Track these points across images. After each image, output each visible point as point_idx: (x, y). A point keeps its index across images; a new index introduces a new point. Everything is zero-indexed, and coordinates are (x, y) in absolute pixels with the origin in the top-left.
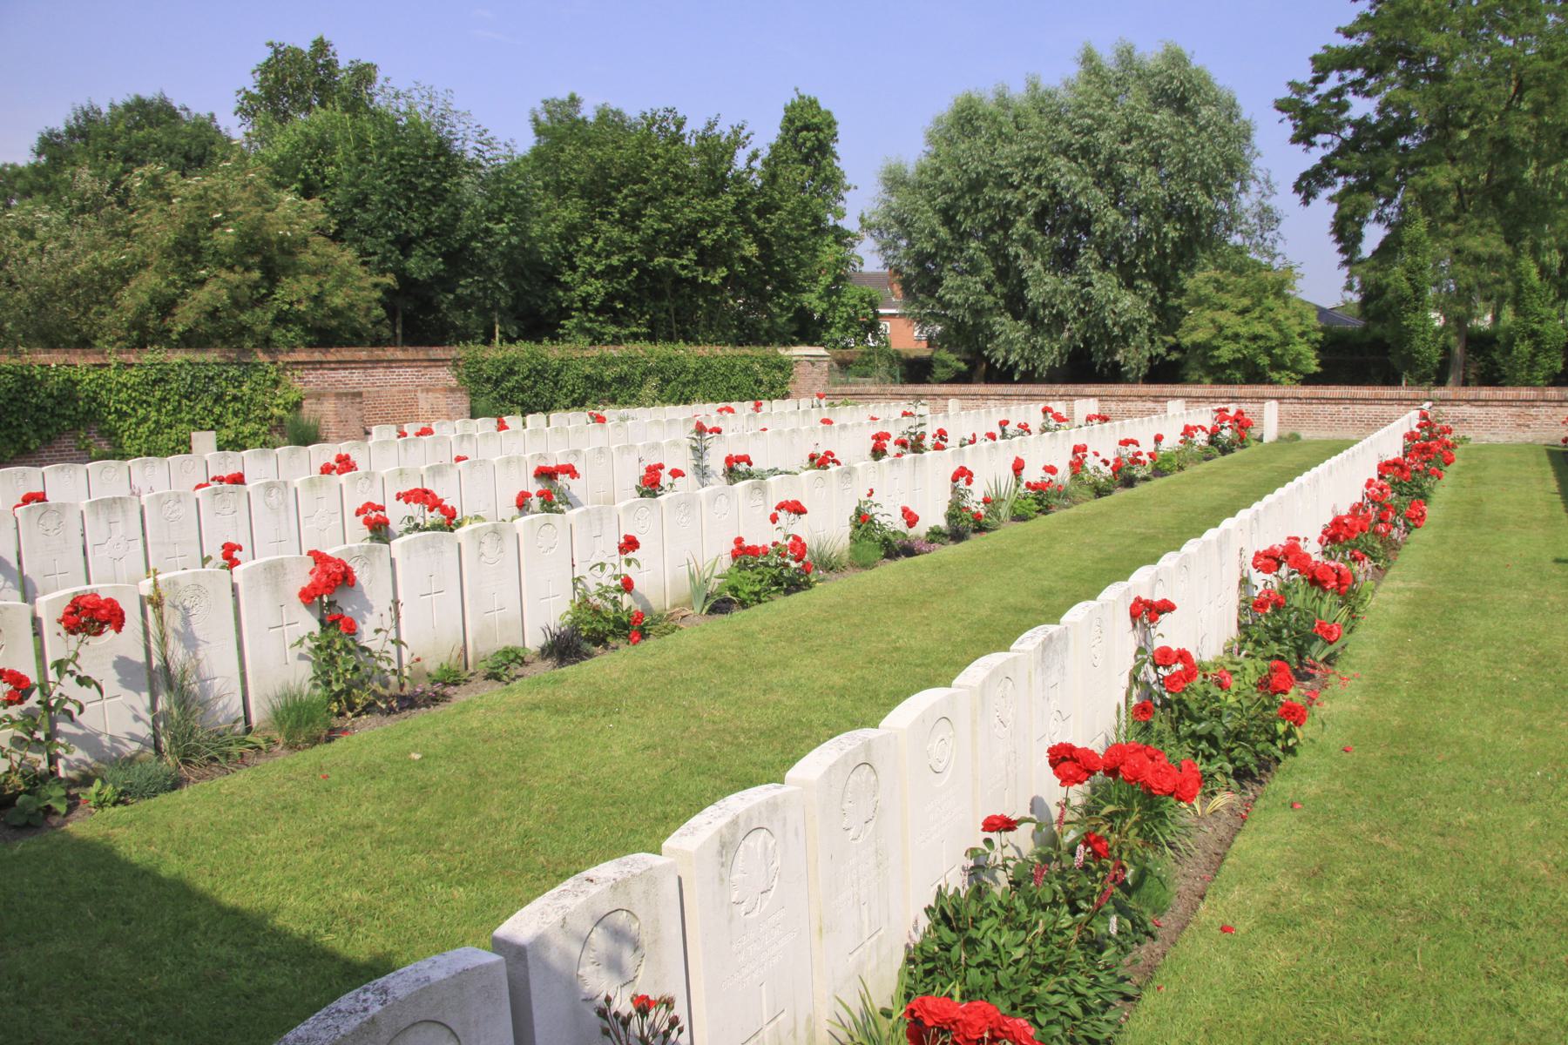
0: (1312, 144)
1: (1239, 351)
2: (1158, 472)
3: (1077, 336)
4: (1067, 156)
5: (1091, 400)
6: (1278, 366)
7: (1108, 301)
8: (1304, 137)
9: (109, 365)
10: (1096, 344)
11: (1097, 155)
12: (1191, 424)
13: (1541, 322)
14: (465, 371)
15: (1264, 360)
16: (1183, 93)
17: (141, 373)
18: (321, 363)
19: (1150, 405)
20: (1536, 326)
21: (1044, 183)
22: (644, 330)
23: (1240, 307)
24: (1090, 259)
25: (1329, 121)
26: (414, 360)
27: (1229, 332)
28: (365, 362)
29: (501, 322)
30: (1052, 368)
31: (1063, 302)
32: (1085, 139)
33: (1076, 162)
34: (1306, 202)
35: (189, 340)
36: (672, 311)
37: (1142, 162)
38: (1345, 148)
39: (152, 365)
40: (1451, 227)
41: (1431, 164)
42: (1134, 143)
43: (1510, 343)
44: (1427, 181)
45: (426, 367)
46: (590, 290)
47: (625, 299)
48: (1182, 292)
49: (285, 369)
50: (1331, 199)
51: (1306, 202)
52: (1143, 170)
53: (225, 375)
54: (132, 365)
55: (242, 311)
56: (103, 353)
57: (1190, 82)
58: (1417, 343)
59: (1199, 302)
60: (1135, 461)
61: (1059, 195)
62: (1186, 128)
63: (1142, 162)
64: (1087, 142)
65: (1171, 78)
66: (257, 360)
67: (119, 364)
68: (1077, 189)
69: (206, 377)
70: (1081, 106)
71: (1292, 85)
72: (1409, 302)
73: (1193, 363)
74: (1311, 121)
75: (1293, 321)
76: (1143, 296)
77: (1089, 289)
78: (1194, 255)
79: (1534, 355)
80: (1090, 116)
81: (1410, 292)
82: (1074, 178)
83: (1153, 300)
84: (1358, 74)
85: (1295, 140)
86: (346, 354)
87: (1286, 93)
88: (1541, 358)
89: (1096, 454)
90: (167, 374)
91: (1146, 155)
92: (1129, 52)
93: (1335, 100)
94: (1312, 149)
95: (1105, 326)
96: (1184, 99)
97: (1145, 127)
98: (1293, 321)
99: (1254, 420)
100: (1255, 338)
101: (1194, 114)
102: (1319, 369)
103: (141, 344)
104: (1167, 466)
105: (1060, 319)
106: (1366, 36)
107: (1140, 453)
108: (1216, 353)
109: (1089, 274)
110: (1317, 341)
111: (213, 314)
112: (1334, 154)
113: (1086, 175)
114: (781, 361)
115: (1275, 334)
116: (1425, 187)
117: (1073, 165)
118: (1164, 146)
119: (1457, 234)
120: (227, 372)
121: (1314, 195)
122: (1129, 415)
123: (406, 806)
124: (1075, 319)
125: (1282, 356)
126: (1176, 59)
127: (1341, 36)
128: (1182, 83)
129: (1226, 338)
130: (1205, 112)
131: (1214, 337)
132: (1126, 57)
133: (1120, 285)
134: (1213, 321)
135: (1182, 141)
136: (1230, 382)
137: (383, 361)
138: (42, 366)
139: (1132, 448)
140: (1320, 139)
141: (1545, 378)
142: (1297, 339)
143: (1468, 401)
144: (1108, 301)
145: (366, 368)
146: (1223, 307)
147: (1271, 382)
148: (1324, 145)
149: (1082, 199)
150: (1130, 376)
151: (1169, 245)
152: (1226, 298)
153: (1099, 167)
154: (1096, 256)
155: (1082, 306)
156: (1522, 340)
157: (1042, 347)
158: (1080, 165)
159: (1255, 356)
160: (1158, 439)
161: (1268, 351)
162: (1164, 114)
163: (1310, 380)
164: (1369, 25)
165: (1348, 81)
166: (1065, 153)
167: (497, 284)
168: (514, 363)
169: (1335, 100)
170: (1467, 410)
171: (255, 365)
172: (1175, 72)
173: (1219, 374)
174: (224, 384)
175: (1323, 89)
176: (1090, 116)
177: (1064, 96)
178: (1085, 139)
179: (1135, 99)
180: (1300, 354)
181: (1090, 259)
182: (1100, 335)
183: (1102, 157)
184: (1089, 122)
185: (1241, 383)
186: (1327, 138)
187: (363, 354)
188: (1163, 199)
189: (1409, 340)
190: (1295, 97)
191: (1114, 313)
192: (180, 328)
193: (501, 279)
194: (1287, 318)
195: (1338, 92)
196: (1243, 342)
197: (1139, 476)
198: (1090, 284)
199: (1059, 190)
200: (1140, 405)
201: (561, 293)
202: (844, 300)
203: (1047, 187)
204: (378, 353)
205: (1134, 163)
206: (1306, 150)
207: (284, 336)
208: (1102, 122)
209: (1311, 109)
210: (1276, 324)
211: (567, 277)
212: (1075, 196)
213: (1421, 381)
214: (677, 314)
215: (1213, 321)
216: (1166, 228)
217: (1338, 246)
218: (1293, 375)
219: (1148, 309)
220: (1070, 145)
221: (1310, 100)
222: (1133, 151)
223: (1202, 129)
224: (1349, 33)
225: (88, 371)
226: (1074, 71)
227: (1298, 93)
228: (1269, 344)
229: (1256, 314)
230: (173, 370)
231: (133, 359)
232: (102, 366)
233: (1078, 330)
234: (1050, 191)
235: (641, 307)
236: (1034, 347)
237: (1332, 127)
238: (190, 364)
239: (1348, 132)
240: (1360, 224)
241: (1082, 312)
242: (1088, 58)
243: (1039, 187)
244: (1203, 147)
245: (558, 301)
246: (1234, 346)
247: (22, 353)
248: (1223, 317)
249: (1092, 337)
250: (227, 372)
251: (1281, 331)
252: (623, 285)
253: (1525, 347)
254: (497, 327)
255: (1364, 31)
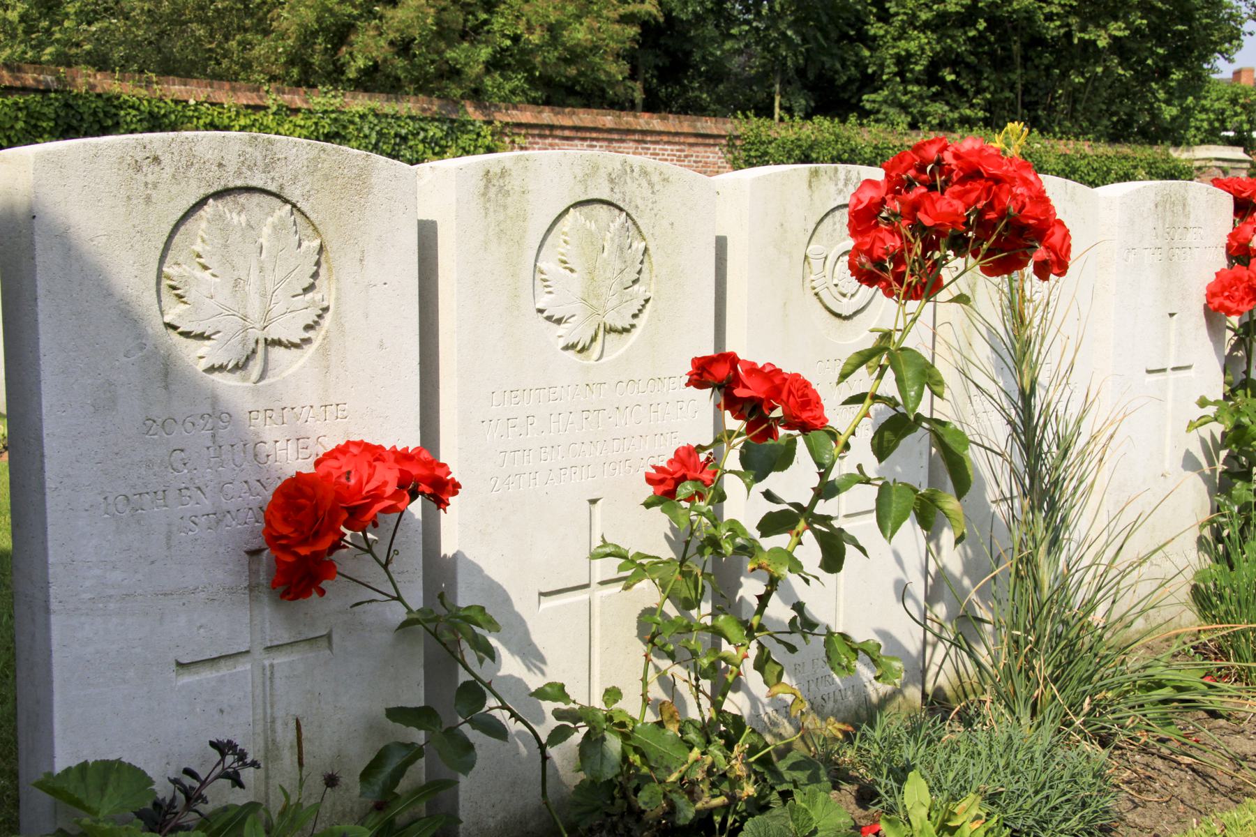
9: (266, 108)
14: (743, 154)
17: (309, 123)
18: (552, 127)
22: (981, 114)
26: (677, 134)
28: (610, 131)
29: (783, 94)
35: (373, 79)
36: (1019, 86)
39: (325, 112)
45: (691, 145)
46: (913, 46)
47: (956, 62)
49: (503, 134)
53: (422, 135)
54: (296, 111)
55: (450, 45)
56: (258, 90)
66: (467, 118)
67: (280, 107)
69: (397, 135)
86: (585, 117)
90: (345, 127)
103: (306, 81)
111: (404, 47)
114: (1175, 167)
120: (425, 130)
137: (634, 132)
138: (176, 102)
145: (610, 141)
167: (784, 34)
168: (811, 147)
171: (464, 124)
174: (421, 147)
187: (607, 119)
192: (361, 63)
193: (789, 27)
201: (867, 53)
202: (1207, 103)
204: (628, 120)
207: (499, 87)
211: (876, 29)
214: (1026, 91)
225: (238, 114)
230: (352, 122)
231: (298, 102)
232: (257, 108)
235: (979, 80)
238: (376, 115)
245: (860, 65)
247: (149, 83)
250: (425, 130)
252: (960, 43)
254: (777, 99)
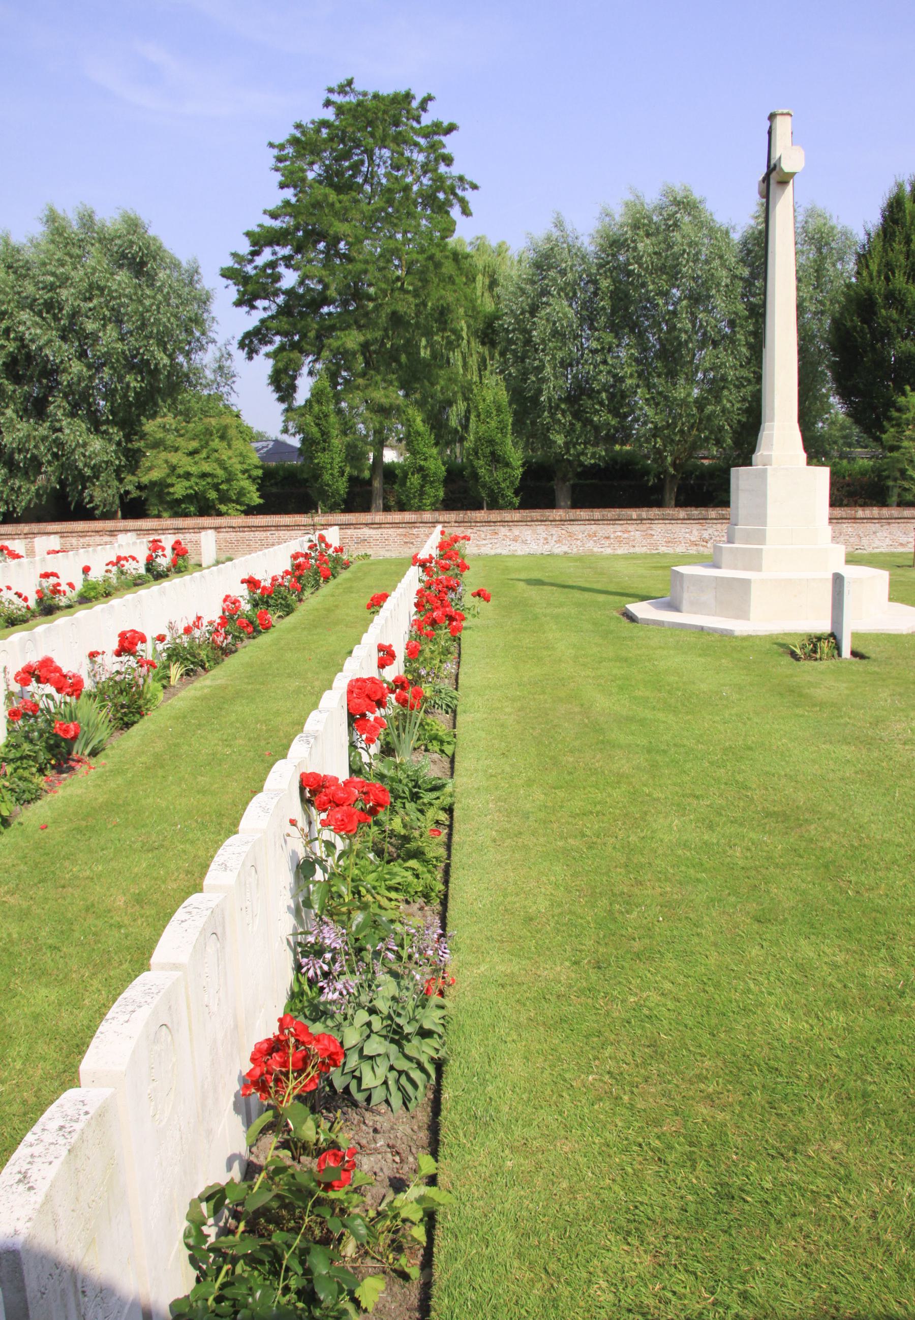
0: (253, 307)
1: (191, 487)
2: (85, 599)
3: (53, 478)
4: (33, 310)
5: (52, 536)
6: (224, 498)
7: (78, 445)
8: (246, 301)
10: (70, 485)
11: (61, 310)
12: (123, 555)
13: (425, 460)
15: (213, 495)
16: (142, 258)
19: (107, 539)
20: (422, 463)
21: (12, 336)
23: (191, 449)
24: (59, 406)
25: (265, 290)
27: (181, 471)
30: (27, 508)
31: (36, 447)
32: (50, 295)
33: (41, 316)
34: (250, 358)
37: (104, 319)
38: (285, 311)
40: (360, 381)
41: (342, 330)
42: (95, 301)
43: (405, 476)
44: (340, 343)
48: (143, 436)
50: (267, 355)
51: (250, 358)
52: (104, 326)
57: (147, 248)
58: (327, 477)
59: (157, 445)
60: (56, 591)
61: (27, 346)
62: (143, 290)
63: (104, 319)
64: (52, 298)
65: (132, 243)
68: (42, 342)
70: (44, 264)
71: (235, 255)
72: (318, 443)
73: (153, 500)
74: (250, 288)
75: (234, 460)
76: (110, 440)
77: (59, 434)
78: (156, 404)
79: (423, 486)
80: (53, 274)
81: (318, 435)
82: (39, 331)
83: (119, 444)
84: (287, 251)
85: (239, 303)
87: (229, 263)
88: (427, 488)
89: (9, 588)
91: (107, 313)
92: (90, 216)
93: (269, 271)
94: (254, 312)
95: (77, 467)
96: (143, 264)
97: (106, 286)
98: (234, 460)
99: (189, 548)
100: (204, 475)
101: (151, 279)
102: (261, 501)
104: (93, 594)
105: (35, 465)
106: (287, 219)
107: (59, 585)
108: (171, 490)
109: (59, 421)
110: (258, 477)
112: (272, 317)
113: (50, 328)
115: (220, 472)
116: (338, 348)
117: (37, 319)
118: (122, 305)
119: (367, 387)
121: (257, 352)
122: (86, 546)
123: (568, 778)
124: (49, 462)
125: (228, 490)
126: (133, 225)
127: (267, 217)
128: (140, 249)
129: (179, 476)
130: (162, 275)
131: (168, 476)
132: (87, 221)
133: (89, 430)
134: (166, 462)
135: (140, 302)
136: (186, 515)
139: (53, 580)
140: (260, 303)
141: (433, 504)
142: (240, 476)
143: (367, 524)
144: (78, 445)
146: (176, 450)
147: (220, 514)
148: (265, 309)
149: (47, 351)
150: (97, 512)
151: (132, 394)
152: (181, 442)
153: (62, 322)
154: (65, 404)
155: (55, 450)
156: (413, 474)
157: (20, 487)
158: (44, 319)
159: (205, 491)
160: (86, 570)
161: (216, 487)
162: (123, 276)
163: (251, 511)
164: (289, 210)
165: (280, 256)
166: (31, 307)
169: (269, 271)
170: (366, 531)
172: (134, 238)
173: (177, 508)
175: (260, 261)
176: (53, 274)
177: (29, 254)
178: (50, 295)
179: (94, 258)
180: (243, 488)
181: (59, 406)
182: (74, 477)
183: (64, 312)
184: (52, 279)
185: (195, 515)
186: (266, 303)
188: (123, 352)
189: (320, 475)
190: (237, 266)
191: (84, 456)
194: (230, 458)
195: (273, 265)
196: (193, 479)
197: (62, 604)
198: (60, 430)
199: (26, 342)
200: (98, 539)
203: (15, 339)
205: (95, 319)
206: (248, 312)
208: (64, 281)
209: (251, 277)
210: (221, 464)
212: (40, 349)
213: (332, 509)
215: (166, 462)
216: (128, 378)
217: (276, 396)
218: (238, 507)
219: (115, 452)
220: (35, 300)
221: (250, 269)
222: (95, 308)
223: (160, 289)
224: (274, 216)
226: (39, 230)
227: (239, 263)
228: (215, 480)
229: (204, 454)
233: (54, 472)
234: (18, 343)
236: (12, 489)
237: (267, 293)
239: (281, 300)
240: (294, 378)
241: (55, 455)
242: (52, 218)
243: (8, 339)
244: (159, 308)
246: (187, 484)
248: (174, 458)
249: (67, 479)
251: (225, 469)
253: (415, 480)
255: (286, 215)
